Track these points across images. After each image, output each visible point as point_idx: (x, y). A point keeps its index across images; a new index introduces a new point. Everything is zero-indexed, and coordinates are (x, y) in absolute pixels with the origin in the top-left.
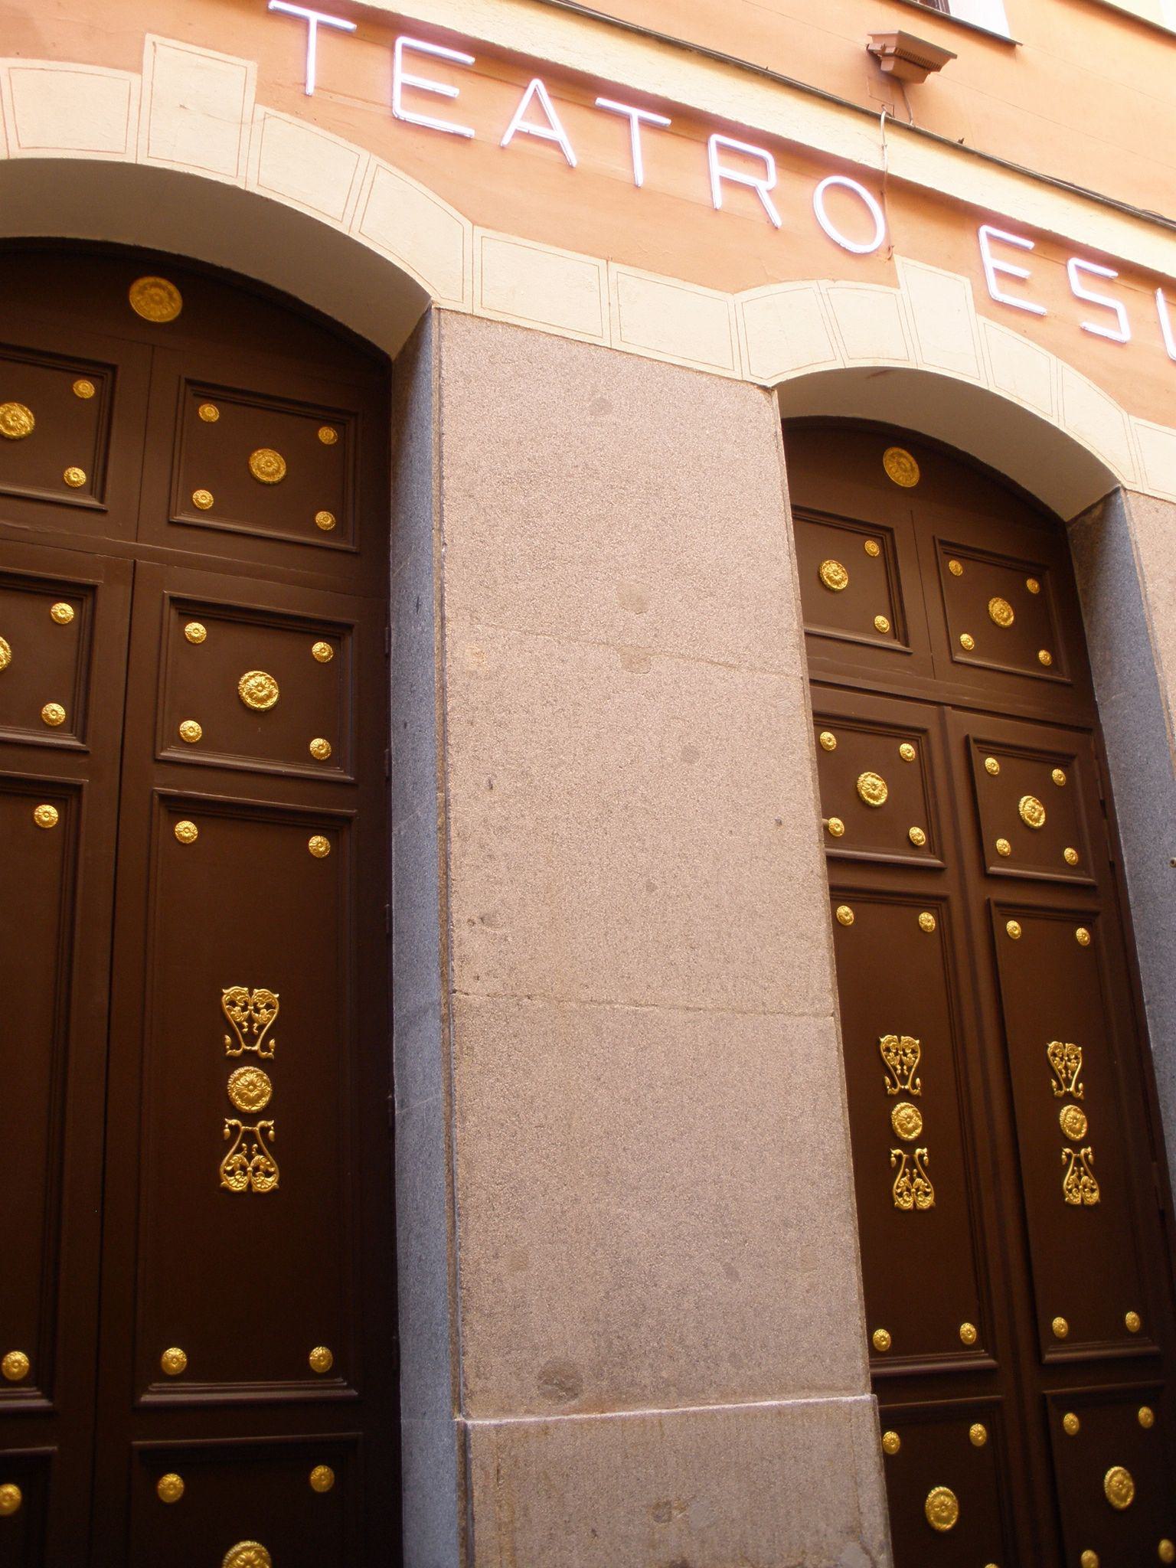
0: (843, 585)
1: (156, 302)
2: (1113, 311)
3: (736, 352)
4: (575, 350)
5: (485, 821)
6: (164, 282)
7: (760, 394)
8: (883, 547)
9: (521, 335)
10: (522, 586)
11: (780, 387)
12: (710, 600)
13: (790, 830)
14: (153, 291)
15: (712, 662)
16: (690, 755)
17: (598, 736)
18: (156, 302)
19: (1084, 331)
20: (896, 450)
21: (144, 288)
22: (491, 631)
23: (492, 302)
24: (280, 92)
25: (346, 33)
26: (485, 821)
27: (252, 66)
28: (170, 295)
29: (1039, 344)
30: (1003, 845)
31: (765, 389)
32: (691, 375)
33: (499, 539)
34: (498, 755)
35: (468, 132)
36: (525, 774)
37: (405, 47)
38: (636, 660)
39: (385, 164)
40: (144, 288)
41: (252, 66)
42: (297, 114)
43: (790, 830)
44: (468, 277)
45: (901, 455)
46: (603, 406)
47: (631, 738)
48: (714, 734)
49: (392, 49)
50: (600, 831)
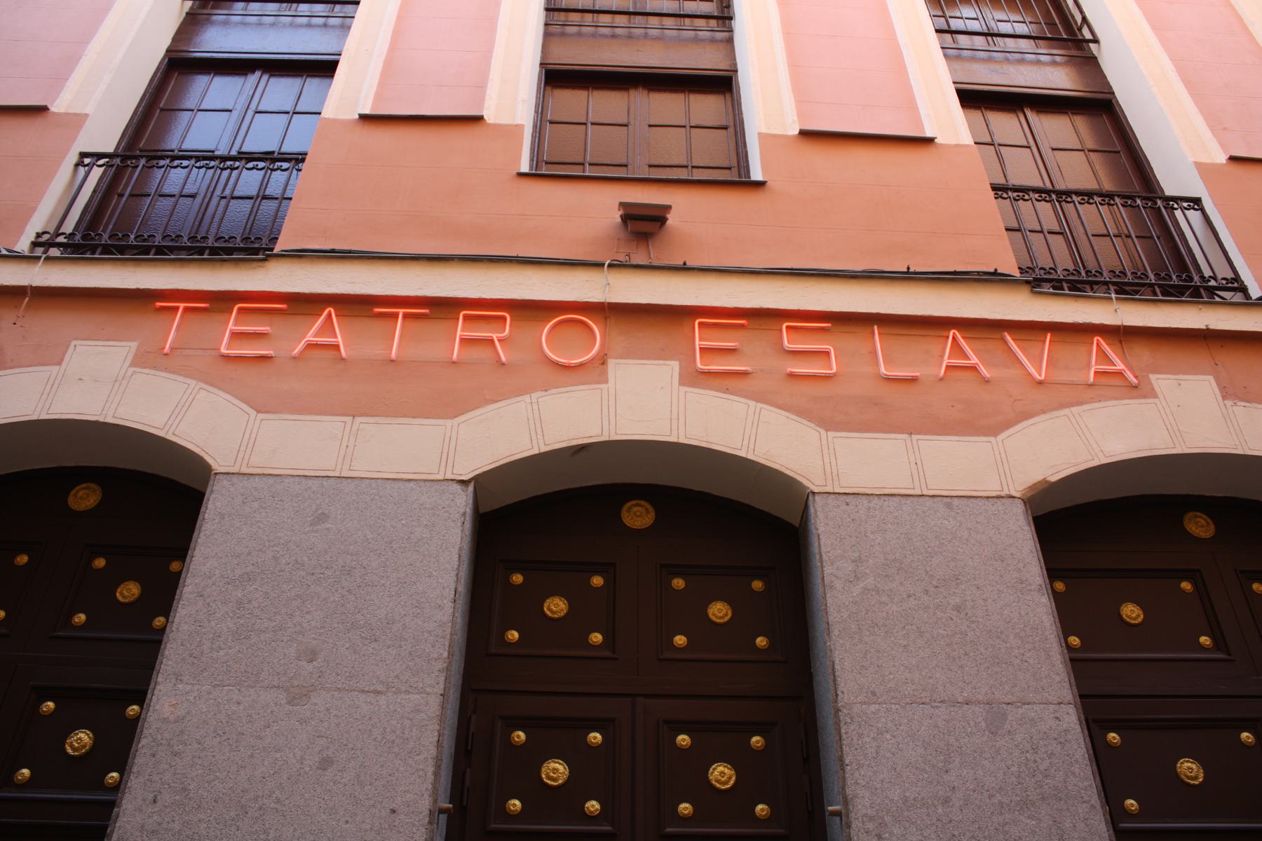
0: (1140, 620)
1: (638, 516)
2: (827, 353)
3: (444, 456)
4: (310, 482)
5: (142, 827)
6: (643, 502)
7: (458, 487)
8: (1195, 585)
9: (271, 480)
10: (222, 653)
11: (476, 479)
12: (374, 645)
13: (402, 817)
14: (635, 509)
15: (363, 691)
16: (326, 763)
17: (252, 756)
18: (638, 516)
19: (792, 376)
20: (1191, 514)
21: (630, 508)
22: (189, 687)
23: (259, 461)
24: (695, 378)
25: (204, 309)
26: (142, 827)
27: (675, 365)
28: (647, 510)
29: (740, 396)
30: (1131, 803)
31: (462, 482)
32: (401, 484)
33: (213, 624)
34: (168, 777)
35: (271, 353)
36: (184, 789)
37: (700, 324)
38: (298, 696)
39: (204, 386)
40: (630, 508)
41: (675, 365)
42: (155, 368)
43: (402, 817)
44: (243, 448)
45: (1196, 517)
46: (322, 518)
47: (278, 755)
48: (350, 746)
49: (781, 330)
50: (234, 828)
